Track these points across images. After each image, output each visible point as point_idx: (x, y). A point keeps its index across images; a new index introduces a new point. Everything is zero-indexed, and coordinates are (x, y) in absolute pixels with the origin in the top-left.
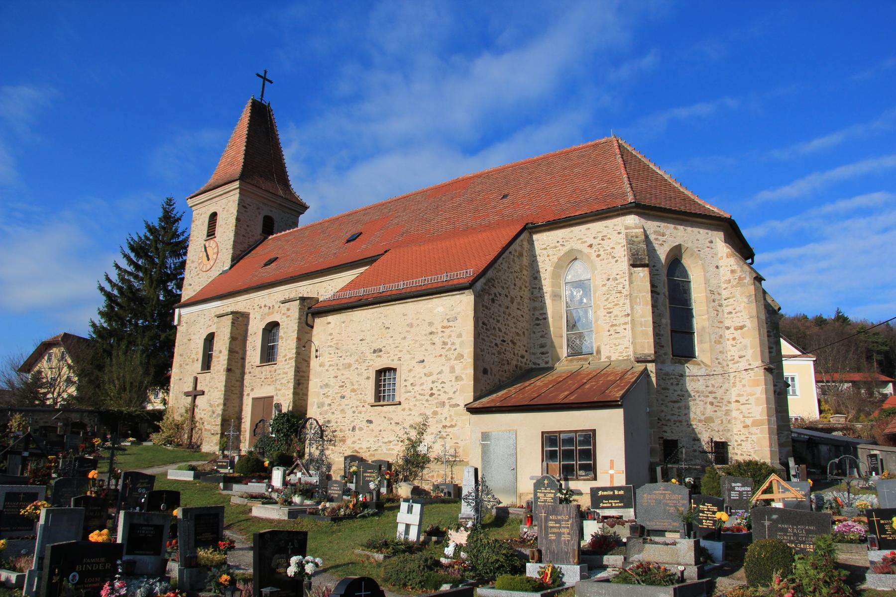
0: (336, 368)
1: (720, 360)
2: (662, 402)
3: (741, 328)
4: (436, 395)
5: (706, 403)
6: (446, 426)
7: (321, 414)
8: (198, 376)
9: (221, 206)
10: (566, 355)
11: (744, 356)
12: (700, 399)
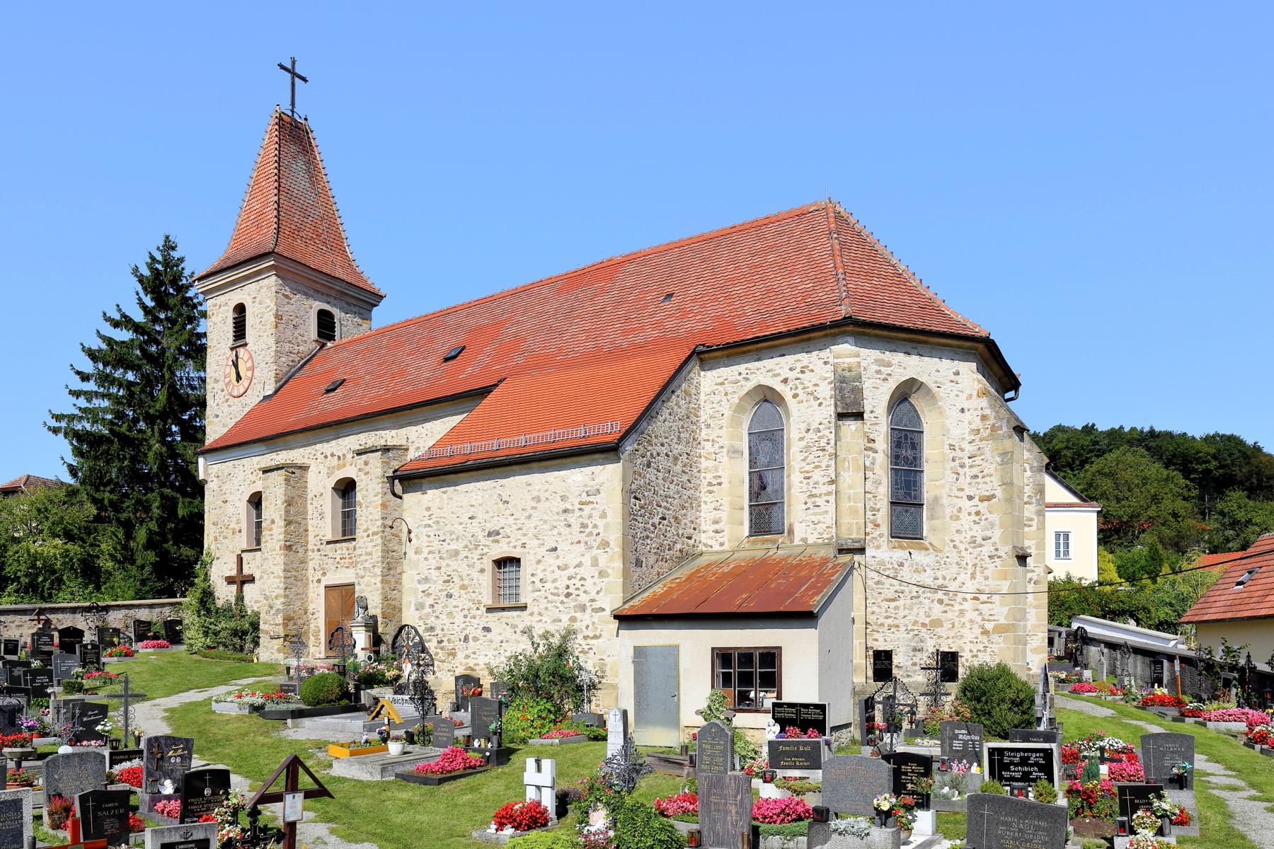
0: (437, 556)
1: (957, 543)
2: (873, 601)
3: (989, 498)
4: (574, 596)
5: (933, 601)
6: (588, 636)
7: (420, 618)
8: (243, 555)
9: (249, 295)
10: (747, 534)
11: (990, 538)
12: (925, 595)
